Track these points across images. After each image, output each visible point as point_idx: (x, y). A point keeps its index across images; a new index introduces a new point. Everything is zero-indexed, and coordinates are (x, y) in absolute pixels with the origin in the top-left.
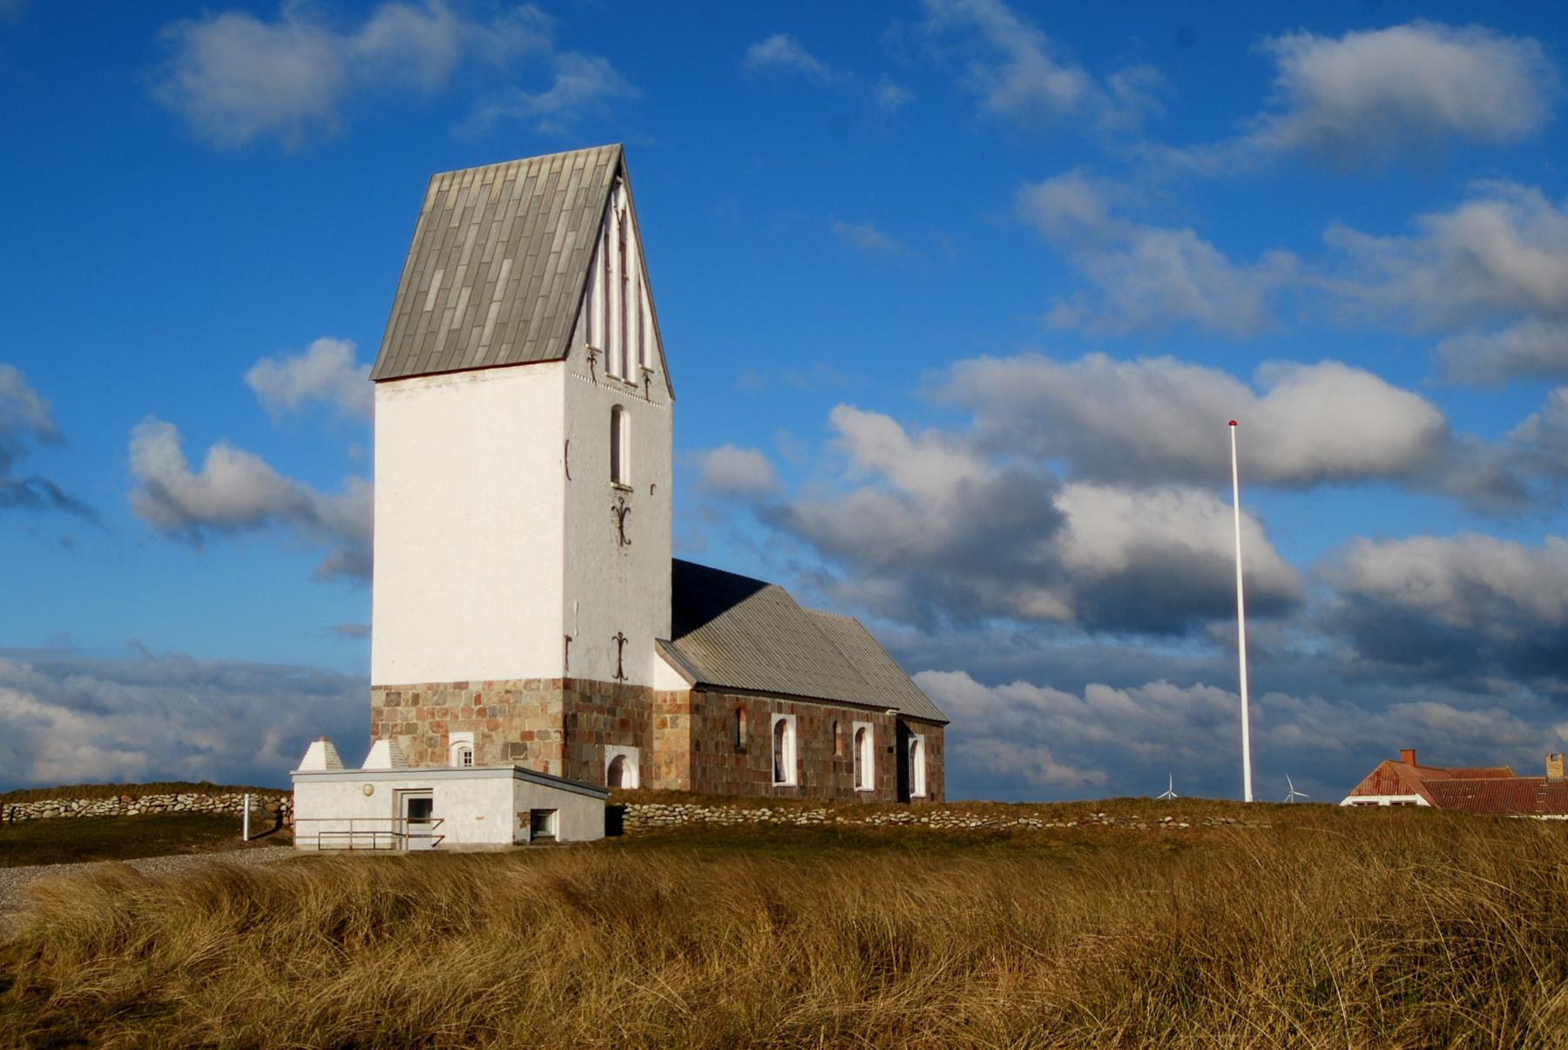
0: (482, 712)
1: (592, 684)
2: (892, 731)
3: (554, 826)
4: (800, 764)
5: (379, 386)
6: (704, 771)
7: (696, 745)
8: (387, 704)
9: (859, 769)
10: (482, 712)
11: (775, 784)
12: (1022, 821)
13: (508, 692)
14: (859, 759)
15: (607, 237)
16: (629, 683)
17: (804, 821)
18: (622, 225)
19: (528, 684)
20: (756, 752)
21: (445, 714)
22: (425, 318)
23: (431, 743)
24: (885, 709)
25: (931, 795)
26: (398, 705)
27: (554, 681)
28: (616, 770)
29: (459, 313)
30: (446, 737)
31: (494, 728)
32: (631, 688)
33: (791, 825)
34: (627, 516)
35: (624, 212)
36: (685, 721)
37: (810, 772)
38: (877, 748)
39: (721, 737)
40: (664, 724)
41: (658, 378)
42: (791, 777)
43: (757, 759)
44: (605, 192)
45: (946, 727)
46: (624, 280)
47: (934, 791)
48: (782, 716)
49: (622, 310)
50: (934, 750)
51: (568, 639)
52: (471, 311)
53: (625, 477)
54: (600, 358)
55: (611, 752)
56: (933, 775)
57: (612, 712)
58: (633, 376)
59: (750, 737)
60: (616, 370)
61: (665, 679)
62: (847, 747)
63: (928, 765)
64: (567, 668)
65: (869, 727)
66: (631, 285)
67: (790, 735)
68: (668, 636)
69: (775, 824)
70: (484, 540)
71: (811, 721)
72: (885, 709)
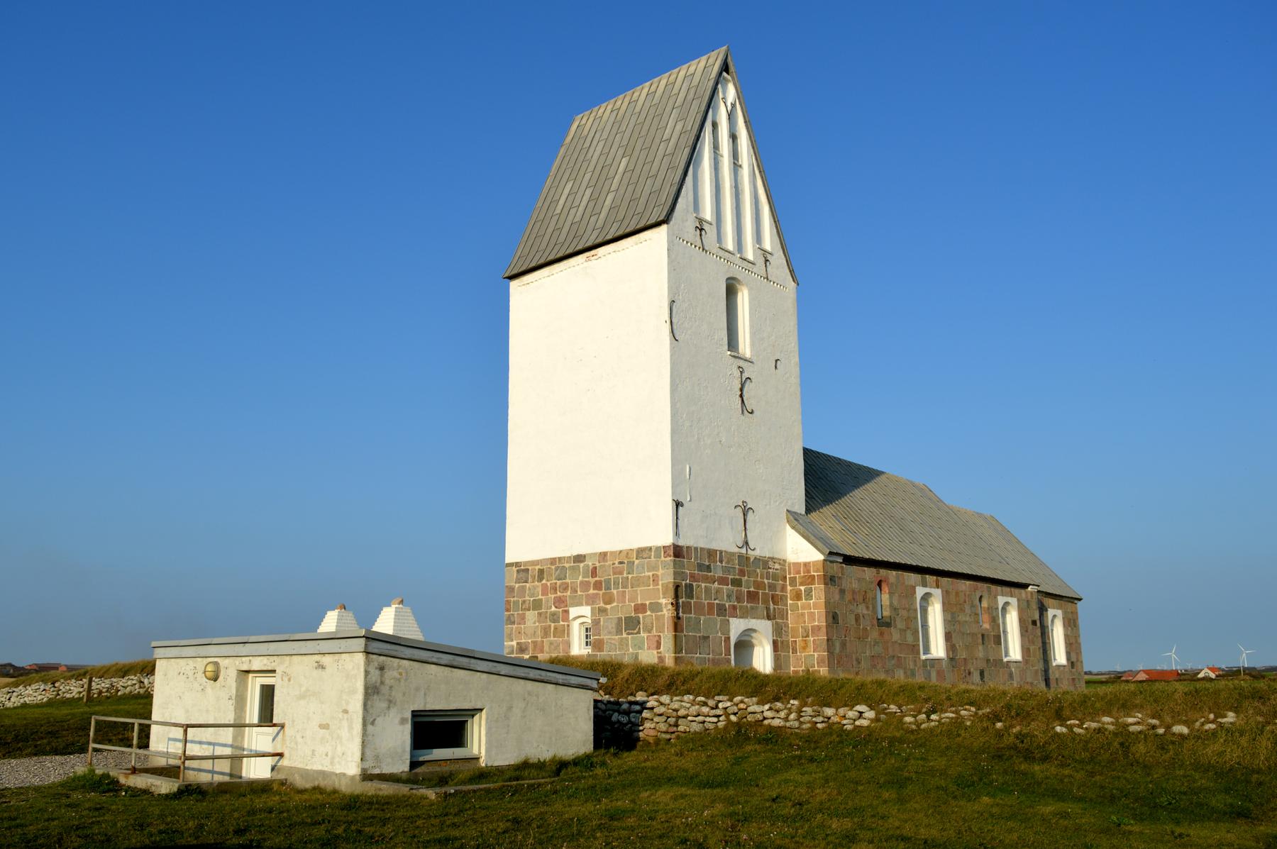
1: (711, 553)
2: (1034, 606)
3: (481, 743)
4: (948, 637)
5: (514, 284)
6: (843, 645)
7: (833, 618)
9: (1006, 641)
10: (598, 586)
11: (923, 657)
14: (1005, 632)
15: (715, 125)
16: (757, 553)
18: (731, 116)
19: (641, 552)
20: (900, 624)
21: (566, 589)
22: (555, 218)
23: (554, 618)
24: (1025, 586)
25: (1072, 664)
28: (744, 646)
29: (581, 209)
30: (567, 612)
35: (733, 105)
36: (819, 589)
37: (959, 644)
38: (1022, 621)
39: (862, 609)
40: (798, 596)
41: (778, 259)
42: (938, 649)
43: (903, 631)
44: (711, 83)
45: (1079, 603)
46: (736, 166)
47: (1074, 659)
48: (927, 590)
49: (729, 182)
50: (1071, 624)
51: (678, 504)
52: (591, 204)
53: (745, 347)
54: (711, 231)
55: (737, 626)
56: (1073, 646)
57: (737, 583)
59: (894, 609)
60: (730, 244)
61: (799, 550)
62: (994, 620)
63: (1066, 637)
64: (677, 534)
65: (1013, 601)
66: (745, 172)
68: (800, 508)
70: (608, 418)
71: (957, 594)
72: (1025, 586)
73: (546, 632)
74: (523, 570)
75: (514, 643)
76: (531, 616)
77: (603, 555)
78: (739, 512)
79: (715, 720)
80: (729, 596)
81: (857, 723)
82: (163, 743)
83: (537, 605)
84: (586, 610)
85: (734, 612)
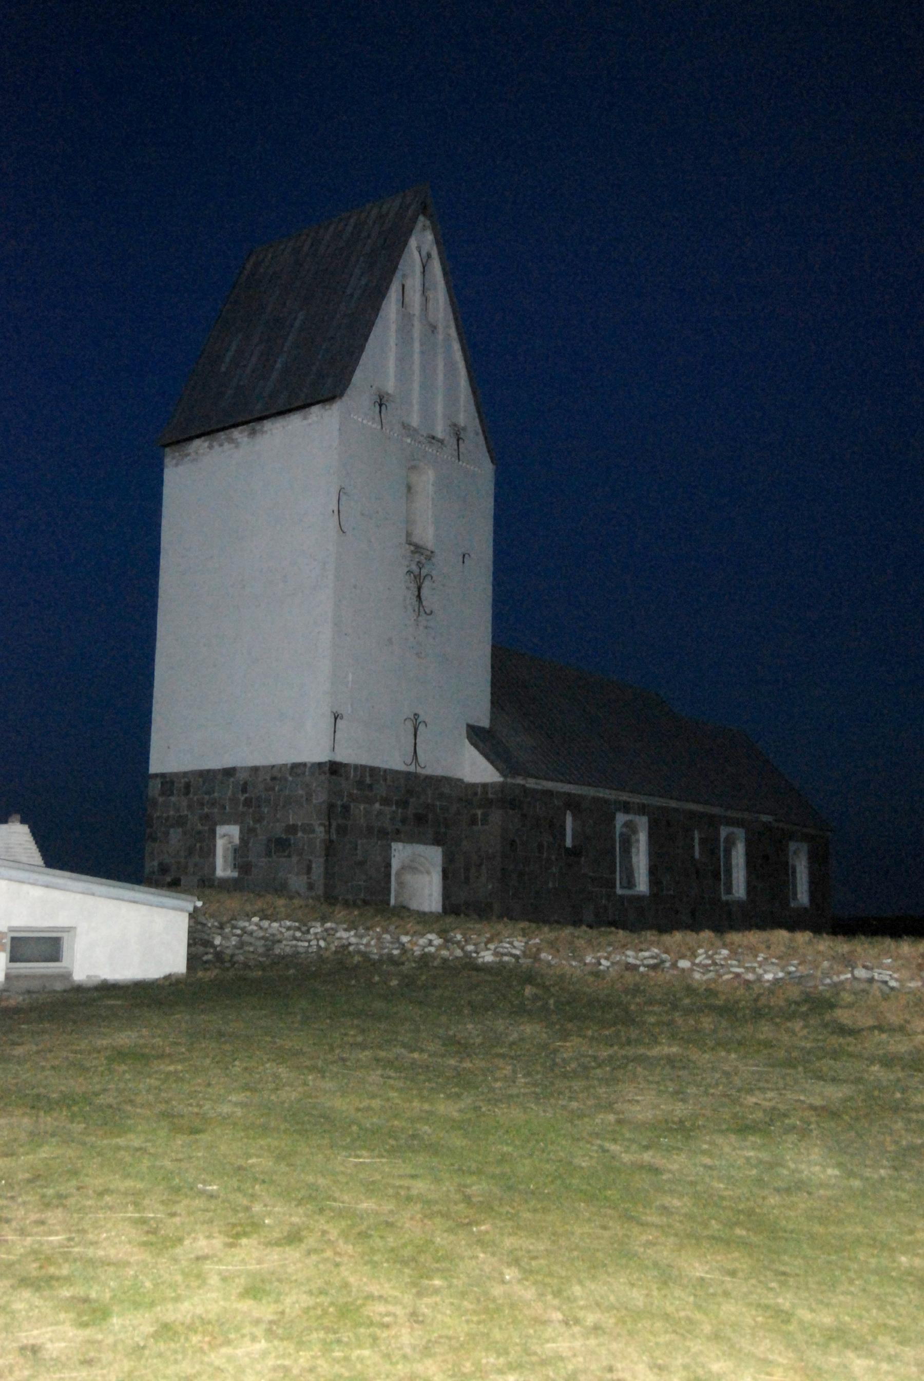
0: (248, 803)
1: (373, 771)
4: (653, 871)
8: (163, 793)
12: (861, 973)
13: (274, 779)
17: (487, 957)
26: (172, 794)
27: (320, 765)
31: (259, 820)
32: (429, 778)
33: (471, 965)
34: (427, 584)
38: (749, 855)
42: (642, 885)
57: (404, 804)
58: (440, 431)
63: (811, 874)
67: (643, 837)
69: (445, 960)
73: (190, 852)
74: (168, 781)
75: (156, 863)
76: (175, 835)
77: (255, 770)
78: (410, 726)
79: (306, 944)
80: (392, 819)
81: (426, 950)
82: (898, 1068)
83: (181, 822)
84: (234, 831)
85: (398, 835)
